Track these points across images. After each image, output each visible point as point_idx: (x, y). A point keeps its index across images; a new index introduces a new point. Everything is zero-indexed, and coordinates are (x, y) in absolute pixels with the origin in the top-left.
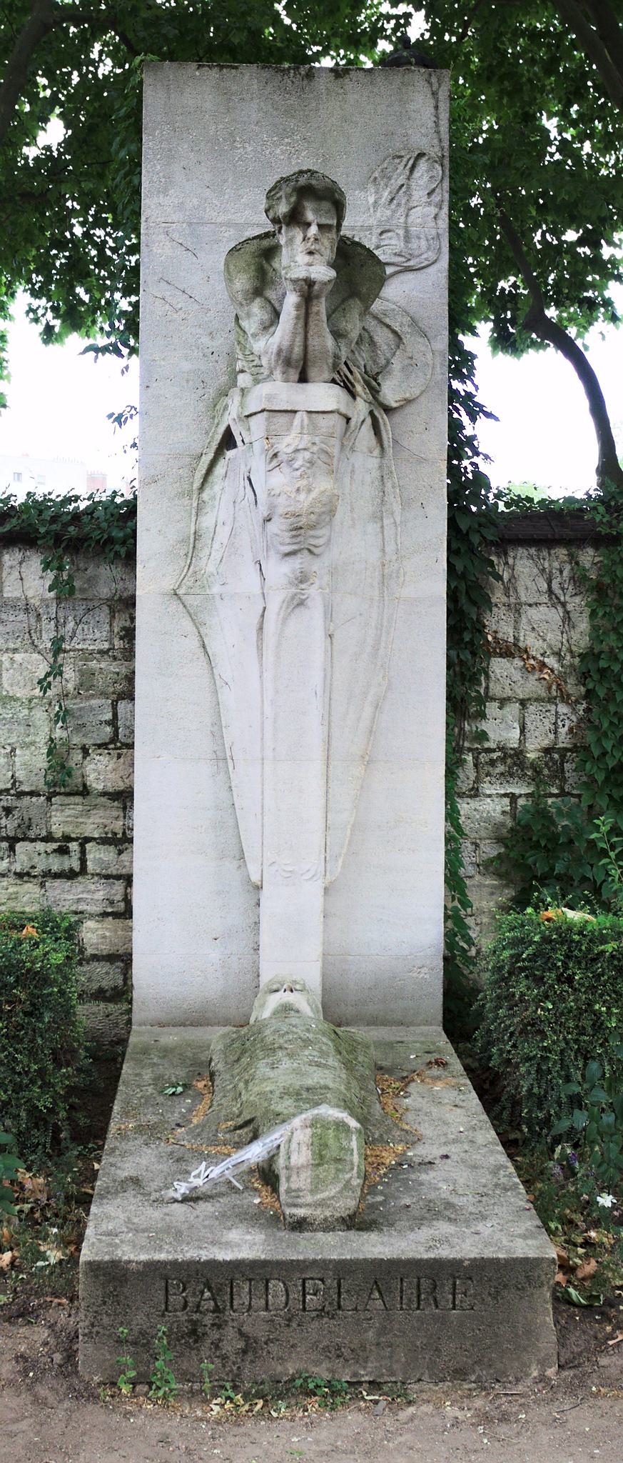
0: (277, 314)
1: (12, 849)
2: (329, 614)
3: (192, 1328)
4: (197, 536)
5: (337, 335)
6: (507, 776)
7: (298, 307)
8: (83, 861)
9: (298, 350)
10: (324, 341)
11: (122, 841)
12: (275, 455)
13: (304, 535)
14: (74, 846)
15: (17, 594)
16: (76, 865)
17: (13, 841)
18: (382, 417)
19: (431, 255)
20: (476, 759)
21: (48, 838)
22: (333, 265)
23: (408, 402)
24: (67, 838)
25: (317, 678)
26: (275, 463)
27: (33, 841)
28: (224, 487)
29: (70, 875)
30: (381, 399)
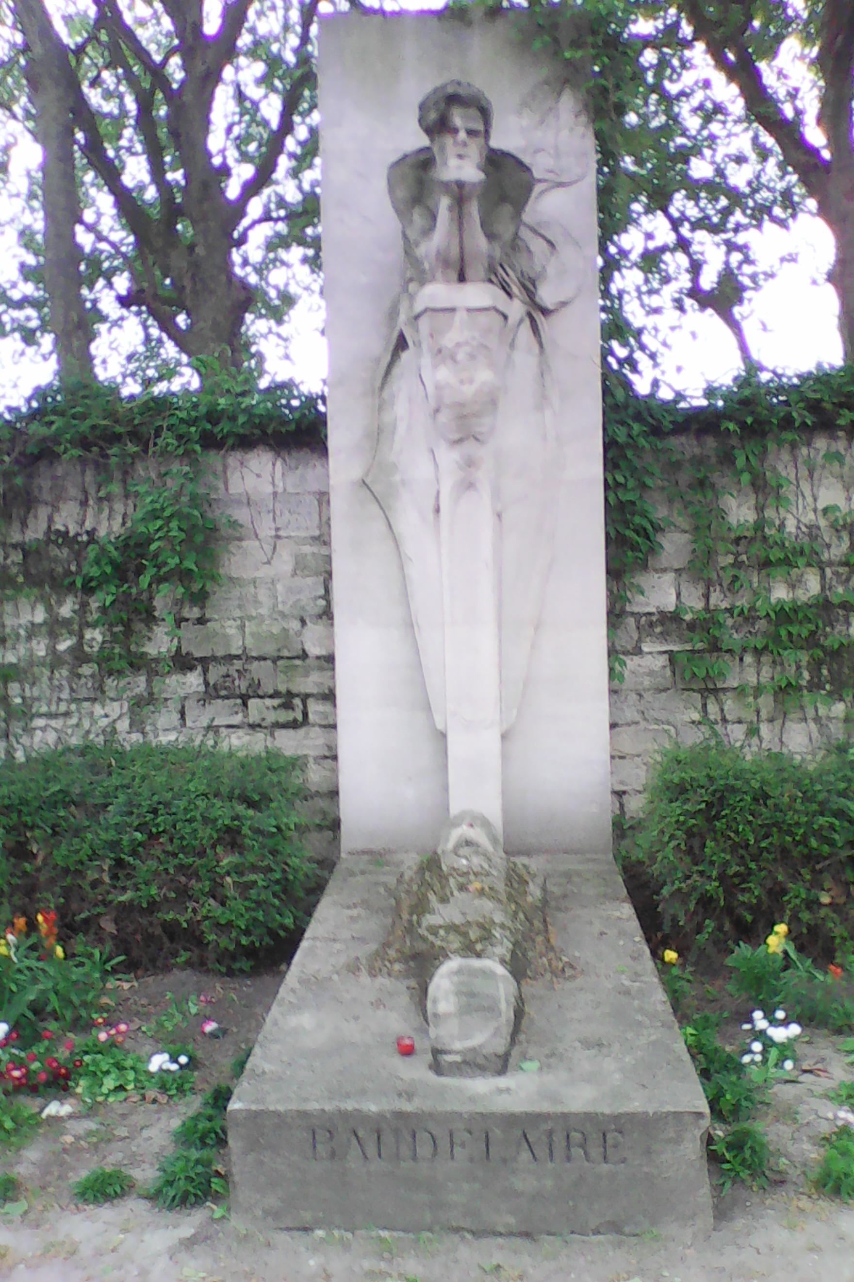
0: (434, 218)
1: (245, 704)
2: (496, 494)
3: (369, 1161)
5: (491, 236)
6: (664, 636)
7: (450, 209)
8: (305, 714)
9: (455, 251)
10: (479, 242)
11: (330, 697)
12: (440, 351)
13: (466, 425)
14: (297, 702)
15: (241, 491)
16: (300, 718)
17: (245, 699)
18: (538, 316)
20: (638, 622)
21: (275, 695)
22: (479, 168)
23: (564, 304)
24: (290, 695)
28: (403, 385)
29: (294, 725)
30: (537, 299)
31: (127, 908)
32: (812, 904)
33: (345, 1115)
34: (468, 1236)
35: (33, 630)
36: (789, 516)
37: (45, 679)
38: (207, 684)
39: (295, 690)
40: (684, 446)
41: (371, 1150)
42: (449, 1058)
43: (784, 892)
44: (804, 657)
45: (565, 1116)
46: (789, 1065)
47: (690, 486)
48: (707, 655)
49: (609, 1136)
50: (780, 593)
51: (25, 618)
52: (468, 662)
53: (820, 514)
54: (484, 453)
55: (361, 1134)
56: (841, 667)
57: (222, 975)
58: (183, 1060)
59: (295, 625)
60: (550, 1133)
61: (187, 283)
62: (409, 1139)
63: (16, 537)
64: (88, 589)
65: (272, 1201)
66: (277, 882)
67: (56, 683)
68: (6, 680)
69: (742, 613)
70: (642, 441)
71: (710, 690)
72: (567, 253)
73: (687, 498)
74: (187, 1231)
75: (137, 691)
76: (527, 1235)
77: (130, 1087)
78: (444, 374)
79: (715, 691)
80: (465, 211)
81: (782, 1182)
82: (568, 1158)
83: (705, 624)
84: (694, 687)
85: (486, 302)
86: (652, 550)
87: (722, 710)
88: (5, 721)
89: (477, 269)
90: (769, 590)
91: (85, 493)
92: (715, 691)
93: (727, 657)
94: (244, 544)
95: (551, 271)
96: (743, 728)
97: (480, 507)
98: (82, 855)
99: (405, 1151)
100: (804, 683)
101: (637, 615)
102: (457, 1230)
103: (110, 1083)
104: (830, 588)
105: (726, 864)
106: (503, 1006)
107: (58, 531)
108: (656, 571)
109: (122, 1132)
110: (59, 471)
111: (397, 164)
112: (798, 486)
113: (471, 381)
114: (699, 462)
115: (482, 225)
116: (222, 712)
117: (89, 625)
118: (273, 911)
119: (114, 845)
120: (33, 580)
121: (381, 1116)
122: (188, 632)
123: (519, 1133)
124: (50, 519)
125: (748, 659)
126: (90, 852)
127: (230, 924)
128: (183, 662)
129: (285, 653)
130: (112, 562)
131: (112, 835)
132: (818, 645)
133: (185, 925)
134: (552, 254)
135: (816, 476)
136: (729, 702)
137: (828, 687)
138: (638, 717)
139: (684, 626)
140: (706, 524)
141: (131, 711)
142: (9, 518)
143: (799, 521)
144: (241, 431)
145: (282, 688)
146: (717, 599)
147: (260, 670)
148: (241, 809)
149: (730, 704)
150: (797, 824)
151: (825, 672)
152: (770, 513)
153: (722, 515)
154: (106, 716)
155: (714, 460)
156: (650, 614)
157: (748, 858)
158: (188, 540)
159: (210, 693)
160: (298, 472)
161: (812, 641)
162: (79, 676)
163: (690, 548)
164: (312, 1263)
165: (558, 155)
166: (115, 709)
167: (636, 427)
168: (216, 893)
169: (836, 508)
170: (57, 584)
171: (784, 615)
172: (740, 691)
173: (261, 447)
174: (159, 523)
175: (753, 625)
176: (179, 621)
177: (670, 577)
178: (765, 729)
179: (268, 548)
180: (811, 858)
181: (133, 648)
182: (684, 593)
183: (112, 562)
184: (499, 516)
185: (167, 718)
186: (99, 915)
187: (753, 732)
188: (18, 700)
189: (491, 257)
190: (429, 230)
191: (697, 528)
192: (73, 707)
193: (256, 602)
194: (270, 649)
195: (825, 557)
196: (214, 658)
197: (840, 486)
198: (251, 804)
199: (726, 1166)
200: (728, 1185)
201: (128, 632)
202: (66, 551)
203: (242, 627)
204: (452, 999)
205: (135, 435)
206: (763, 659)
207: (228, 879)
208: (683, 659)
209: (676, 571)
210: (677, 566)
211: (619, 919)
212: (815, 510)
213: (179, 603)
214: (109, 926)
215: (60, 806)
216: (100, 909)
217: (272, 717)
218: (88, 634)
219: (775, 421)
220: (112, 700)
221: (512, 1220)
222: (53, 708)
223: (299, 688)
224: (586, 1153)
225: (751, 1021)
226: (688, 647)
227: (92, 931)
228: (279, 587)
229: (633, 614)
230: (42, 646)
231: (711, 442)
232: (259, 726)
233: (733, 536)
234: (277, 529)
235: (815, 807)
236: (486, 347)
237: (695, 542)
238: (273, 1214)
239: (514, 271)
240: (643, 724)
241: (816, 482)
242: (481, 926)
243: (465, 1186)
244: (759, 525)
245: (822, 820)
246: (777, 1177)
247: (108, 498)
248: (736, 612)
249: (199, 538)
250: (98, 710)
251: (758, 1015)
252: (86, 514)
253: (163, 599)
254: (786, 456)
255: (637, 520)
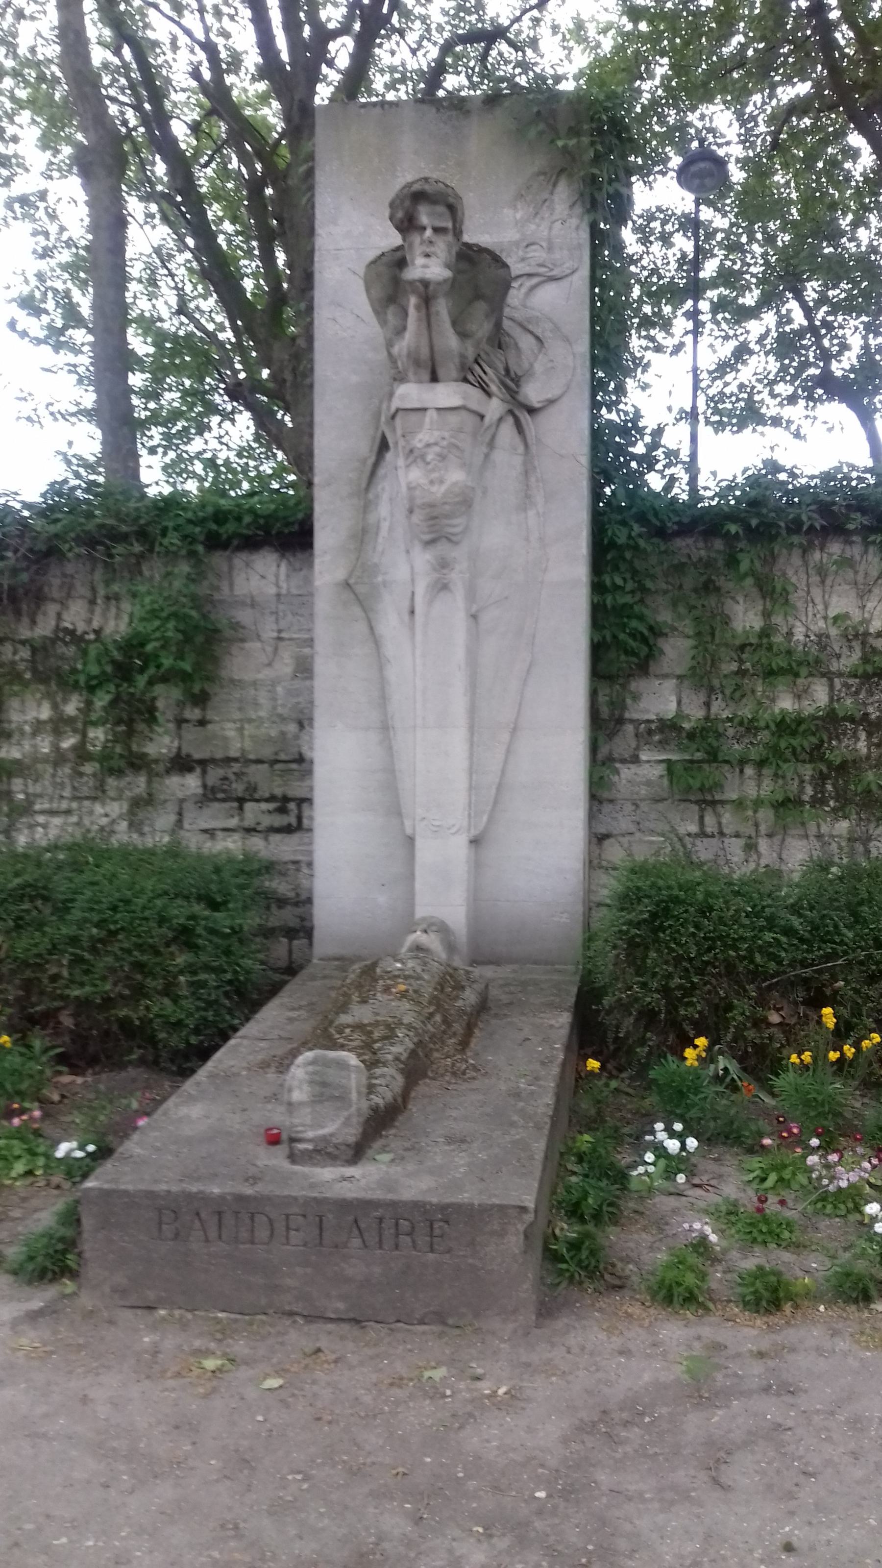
1: (241, 808)
2: (471, 594)
4: (364, 531)
5: (463, 335)
6: (663, 744)
7: (418, 308)
9: (425, 352)
10: (450, 341)
12: (411, 451)
13: (439, 526)
14: (292, 806)
16: (293, 821)
17: (241, 801)
18: (524, 417)
19: (569, 265)
20: (637, 728)
21: (272, 799)
22: (448, 266)
23: (551, 402)
24: (286, 799)
25: (459, 654)
26: (411, 459)
27: (257, 801)
29: (288, 830)
30: (521, 398)
31: (82, 1005)
32: (760, 1023)
33: (190, 1197)
34: (301, 1321)
35: (38, 727)
36: (798, 624)
37: (47, 776)
38: (205, 786)
39: (291, 794)
40: (688, 547)
41: (213, 1234)
42: (301, 1146)
43: (730, 1007)
44: (807, 771)
45: (394, 1204)
46: (681, 1178)
47: (695, 590)
48: (705, 766)
49: (436, 1225)
50: (786, 704)
51: (31, 714)
52: (440, 765)
53: (830, 621)
54: (459, 554)
55: (203, 1215)
56: (846, 782)
57: (173, 1073)
58: (91, 1148)
59: (292, 728)
60: (381, 1220)
61: (288, 376)
62: (248, 1221)
63: (25, 633)
64: (92, 689)
65: (120, 1279)
66: (230, 982)
67: (58, 780)
68: (10, 775)
69: (741, 724)
70: (642, 543)
71: (707, 800)
72: (557, 350)
73: (693, 602)
74: (37, 1304)
75: (137, 791)
76: (356, 1321)
77: (39, 1172)
78: (416, 475)
79: (713, 803)
80: (433, 310)
81: (621, 1287)
82: (397, 1247)
83: (705, 735)
84: (692, 798)
85: (456, 402)
86: (650, 656)
87: (720, 824)
88: (8, 816)
89: (449, 369)
90: (773, 700)
91: (93, 590)
92: (713, 803)
93: (727, 767)
94: (247, 645)
95: (538, 367)
96: (741, 842)
97: (454, 607)
98: (41, 949)
99: (244, 1234)
100: (806, 798)
101: (636, 723)
102: (291, 1314)
103: (19, 1167)
104: (838, 700)
105: (670, 976)
106: (354, 1096)
107: (66, 630)
108: (657, 676)
109: (16, 1213)
110: (70, 568)
111: (374, 262)
112: (808, 592)
113: (441, 482)
114: (709, 564)
115: (454, 324)
116: (215, 816)
117: (94, 724)
118: (223, 1011)
119: (74, 940)
120: (41, 678)
121: (222, 1197)
122: (190, 733)
123: (351, 1218)
124: (59, 616)
125: (749, 771)
126: (49, 947)
127: (179, 1024)
128: (182, 764)
129: (283, 757)
130: (113, 662)
131: (72, 931)
132: (822, 759)
133: (137, 1023)
134: (540, 351)
135: (828, 582)
136: (727, 815)
137: (832, 803)
138: (632, 828)
139: (684, 735)
140: (710, 629)
141: (132, 812)
142: (18, 613)
143: (808, 629)
144: (245, 531)
145: (278, 792)
146: (720, 709)
147: (258, 774)
148: (198, 908)
149: (727, 816)
150: (743, 939)
151: (829, 787)
152: (777, 619)
153: (727, 621)
154: (106, 815)
155: (720, 563)
156: (648, 721)
157: (692, 970)
158: (188, 639)
159: (209, 795)
160: (302, 573)
161: (816, 754)
162: (81, 774)
163: (693, 652)
164: (146, 1339)
165: (550, 249)
166: (116, 808)
167: (637, 528)
168: (168, 991)
169: (846, 616)
170: (61, 681)
171: (786, 726)
172: (739, 804)
173: (267, 548)
174: (157, 623)
175: (755, 735)
176: (180, 722)
177: (671, 683)
178: (763, 845)
179: (269, 649)
180: (755, 975)
181: (135, 748)
182: (685, 700)
183: (113, 662)
184: (474, 617)
185: (164, 820)
186: (58, 1010)
187: (751, 847)
188: (21, 796)
189: (462, 356)
190: (400, 331)
191: (699, 634)
192: (74, 805)
193: (256, 705)
194: (267, 752)
195: (834, 666)
196: (213, 761)
197: (853, 593)
198: (214, 906)
199: (564, 1266)
200: (564, 1285)
201: (131, 733)
202: (73, 648)
203: (241, 730)
204: (306, 1087)
205: (142, 535)
206: (765, 771)
207: (182, 978)
208: (679, 768)
209: (679, 677)
210: (679, 672)
211: (551, 1026)
212: (825, 618)
213: (181, 704)
214: (67, 1021)
215: (26, 899)
216: (56, 1004)
217: (267, 821)
218: (91, 734)
219: (782, 524)
220: (113, 799)
221: (341, 1306)
222: (55, 805)
223: (280, 792)
224: (414, 1242)
225: (653, 1132)
226: (687, 757)
227: (51, 1025)
228: (279, 689)
229: (632, 721)
230: (46, 743)
231: (718, 544)
232: (255, 830)
233: (738, 642)
234: (280, 631)
235: (762, 922)
236: (457, 447)
237: (696, 647)
238: (123, 1292)
239: (495, 369)
240: (638, 835)
241: (828, 588)
242: (388, 1026)
243: (299, 1270)
244: (765, 633)
245: (768, 936)
246: (617, 1282)
247: (117, 597)
248: (736, 721)
249: (199, 639)
250: (99, 809)
251: (659, 1126)
252: (91, 614)
253: (166, 698)
254: (796, 559)
255: (634, 623)
